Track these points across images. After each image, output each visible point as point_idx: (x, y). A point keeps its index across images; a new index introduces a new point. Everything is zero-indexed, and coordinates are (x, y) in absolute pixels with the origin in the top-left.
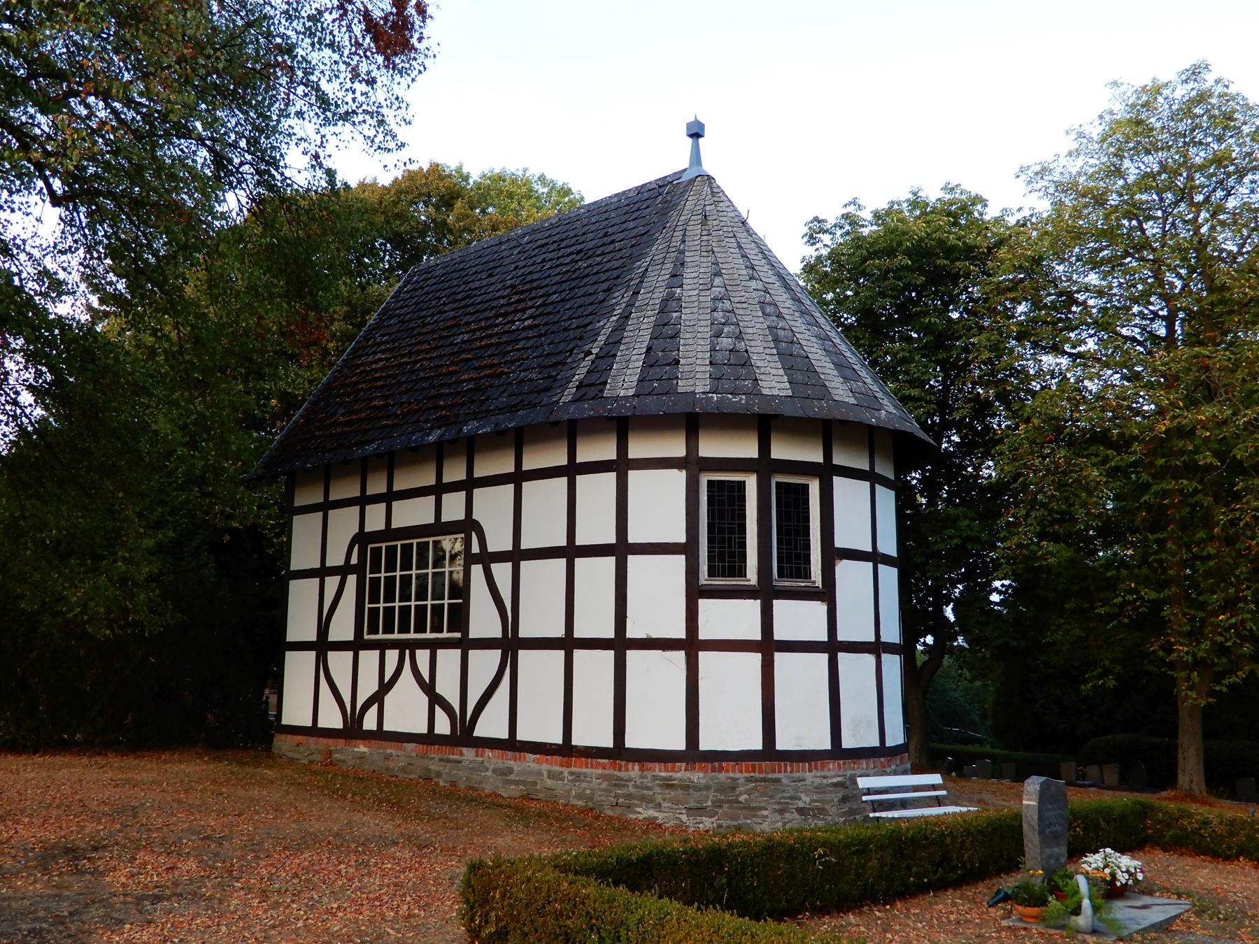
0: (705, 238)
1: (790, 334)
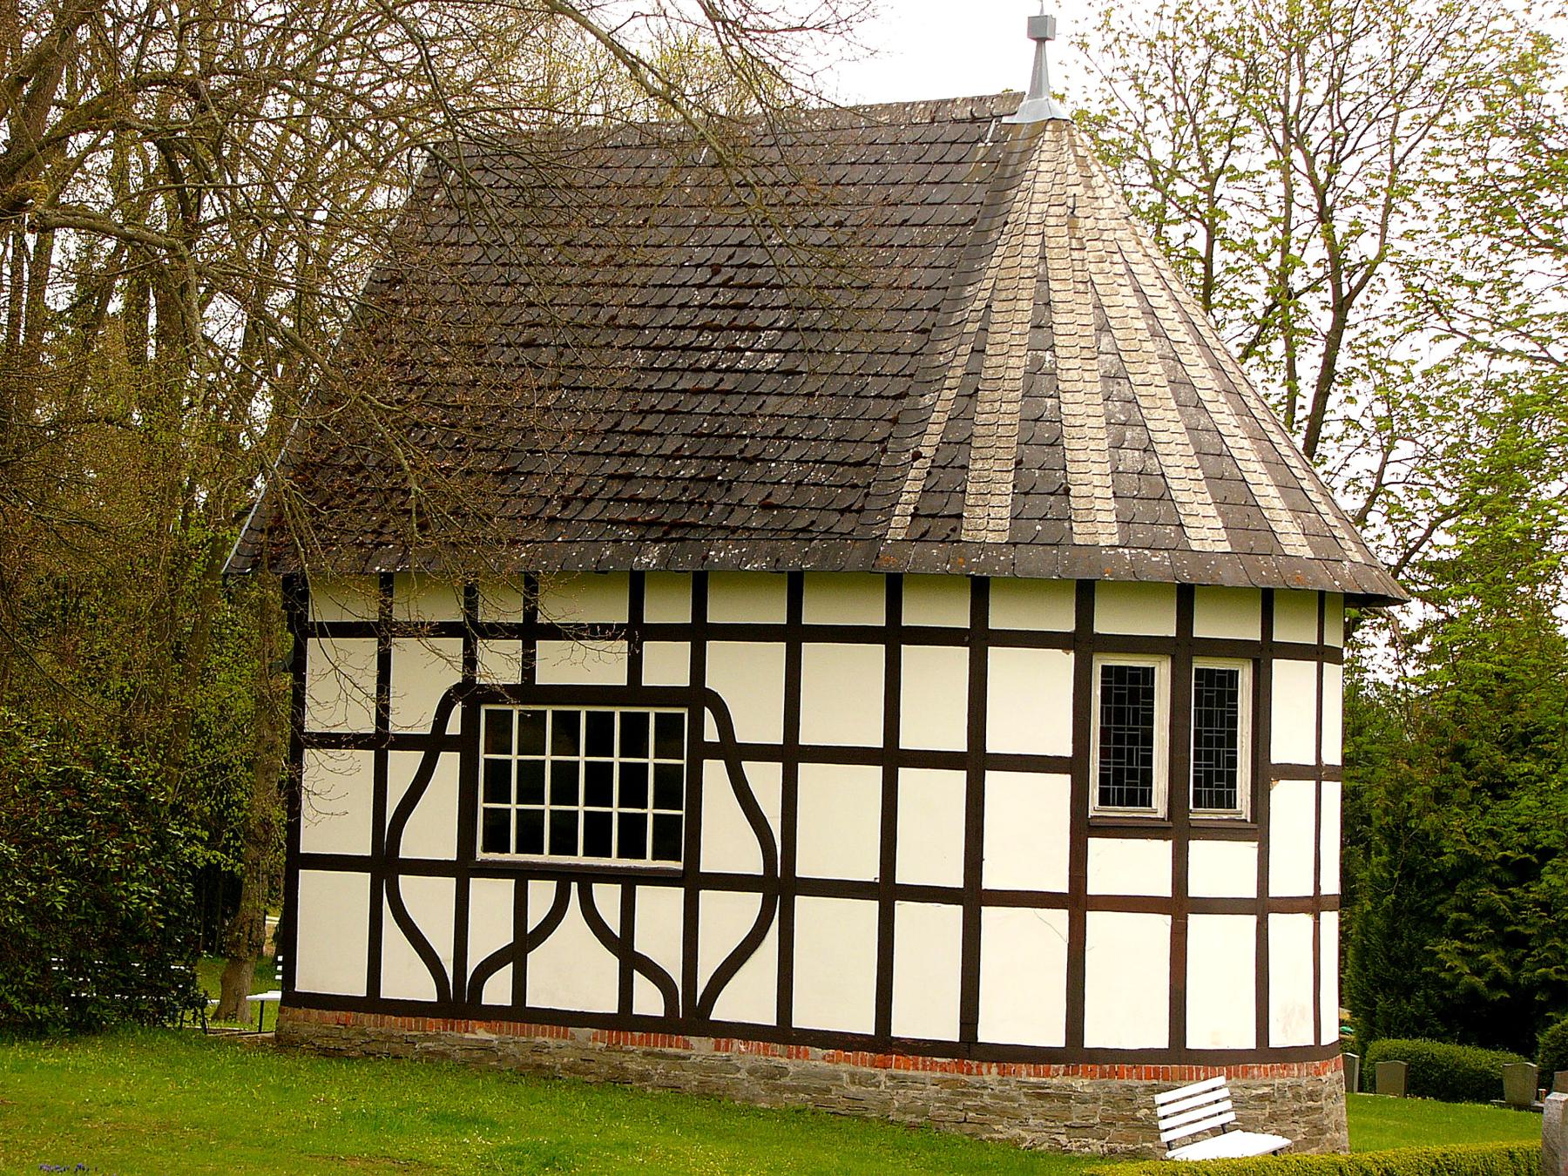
0: (1076, 254)
1: (1217, 439)
